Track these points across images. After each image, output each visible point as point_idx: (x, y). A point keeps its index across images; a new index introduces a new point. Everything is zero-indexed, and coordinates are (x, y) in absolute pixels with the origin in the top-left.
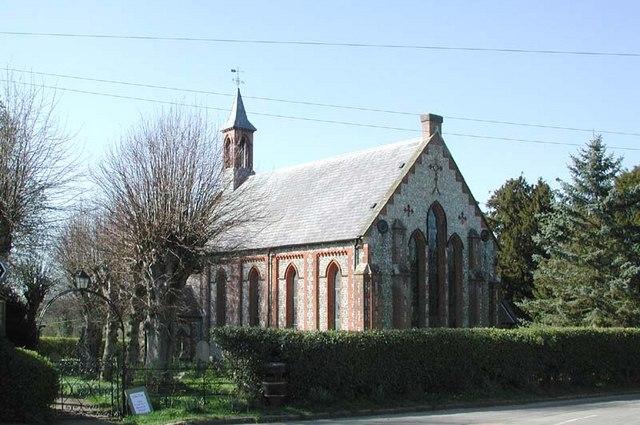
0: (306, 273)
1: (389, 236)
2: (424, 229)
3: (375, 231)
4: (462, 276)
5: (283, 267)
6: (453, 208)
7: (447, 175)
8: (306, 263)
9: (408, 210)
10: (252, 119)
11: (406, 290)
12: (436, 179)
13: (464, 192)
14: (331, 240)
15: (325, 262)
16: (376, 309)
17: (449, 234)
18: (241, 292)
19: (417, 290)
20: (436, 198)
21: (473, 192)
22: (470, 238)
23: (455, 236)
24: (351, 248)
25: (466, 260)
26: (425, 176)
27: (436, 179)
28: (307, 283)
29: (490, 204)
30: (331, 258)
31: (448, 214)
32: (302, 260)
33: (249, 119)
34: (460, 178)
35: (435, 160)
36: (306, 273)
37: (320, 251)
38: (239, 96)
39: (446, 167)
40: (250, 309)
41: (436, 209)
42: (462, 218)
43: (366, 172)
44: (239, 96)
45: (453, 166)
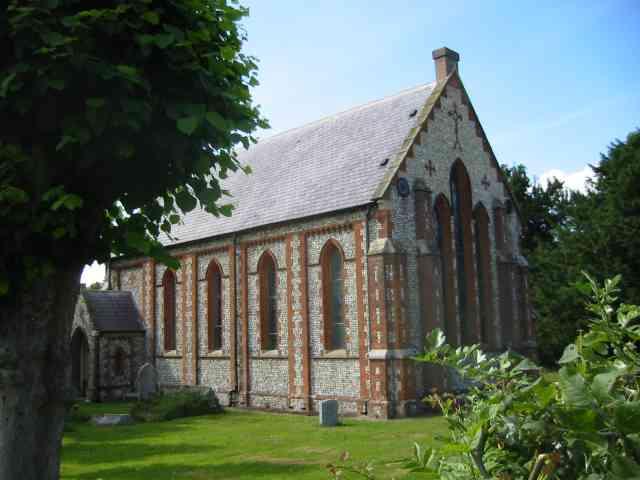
0: (289, 262)
1: (411, 199)
2: (448, 195)
3: (394, 195)
8: (289, 250)
9: (430, 168)
12: (456, 131)
18: (197, 295)
22: (496, 210)
27: (456, 131)
28: (290, 276)
34: (481, 133)
37: (306, 227)
39: (466, 117)
41: (458, 173)
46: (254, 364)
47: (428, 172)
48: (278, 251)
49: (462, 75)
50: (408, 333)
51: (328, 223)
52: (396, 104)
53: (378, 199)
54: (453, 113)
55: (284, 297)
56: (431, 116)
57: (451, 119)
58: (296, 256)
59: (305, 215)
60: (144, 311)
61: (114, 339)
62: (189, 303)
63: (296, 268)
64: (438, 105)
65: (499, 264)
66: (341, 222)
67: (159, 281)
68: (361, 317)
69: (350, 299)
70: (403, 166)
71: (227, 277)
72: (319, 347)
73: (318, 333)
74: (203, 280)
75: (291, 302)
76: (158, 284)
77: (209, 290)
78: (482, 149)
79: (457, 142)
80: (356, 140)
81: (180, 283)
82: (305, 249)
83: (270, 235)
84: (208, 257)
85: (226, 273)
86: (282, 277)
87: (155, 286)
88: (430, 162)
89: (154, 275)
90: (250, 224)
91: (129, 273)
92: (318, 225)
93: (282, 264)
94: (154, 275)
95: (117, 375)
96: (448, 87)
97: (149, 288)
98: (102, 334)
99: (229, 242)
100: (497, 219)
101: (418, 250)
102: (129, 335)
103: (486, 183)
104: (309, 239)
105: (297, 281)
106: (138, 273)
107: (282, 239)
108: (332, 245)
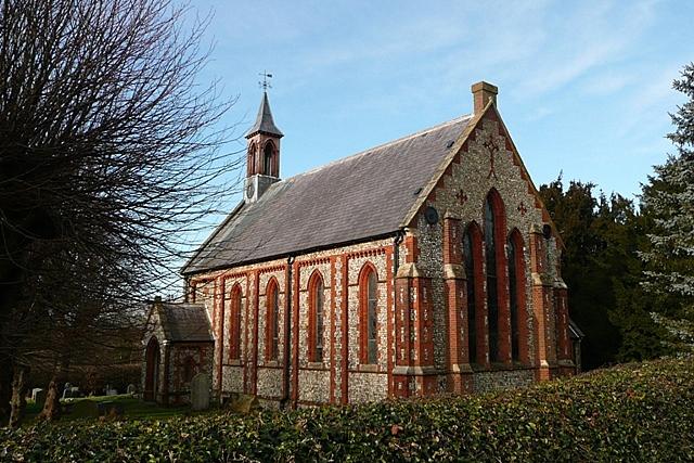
0: (334, 281)
2: (480, 222)
3: (421, 223)
5: (306, 274)
6: (507, 186)
7: (503, 155)
10: (279, 123)
12: (492, 161)
14: (365, 236)
15: (356, 265)
16: (423, 324)
24: (390, 241)
26: (478, 157)
27: (492, 161)
28: (334, 294)
30: (363, 259)
32: (328, 265)
33: (275, 124)
34: (518, 161)
35: (489, 132)
36: (334, 281)
37: (348, 249)
38: (266, 97)
39: (502, 148)
41: (493, 199)
43: (406, 159)
44: (266, 97)
45: (510, 146)
46: (302, 375)
47: (459, 201)
48: (243, 282)
49: (499, 108)
50: (74, 116)
52: (438, 135)
54: (491, 145)
55: (328, 314)
56: (465, 147)
58: (339, 276)
61: (185, 348)
62: (251, 316)
63: (339, 288)
64: (472, 136)
67: (262, 290)
68: (389, 334)
70: (431, 196)
72: (355, 360)
73: (354, 348)
80: (401, 168)
85: (282, 290)
86: (327, 294)
88: (462, 191)
92: (357, 248)
93: (327, 283)
95: (186, 381)
96: (203, 402)
97: (219, 301)
98: (171, 344)
103: (522, 209)
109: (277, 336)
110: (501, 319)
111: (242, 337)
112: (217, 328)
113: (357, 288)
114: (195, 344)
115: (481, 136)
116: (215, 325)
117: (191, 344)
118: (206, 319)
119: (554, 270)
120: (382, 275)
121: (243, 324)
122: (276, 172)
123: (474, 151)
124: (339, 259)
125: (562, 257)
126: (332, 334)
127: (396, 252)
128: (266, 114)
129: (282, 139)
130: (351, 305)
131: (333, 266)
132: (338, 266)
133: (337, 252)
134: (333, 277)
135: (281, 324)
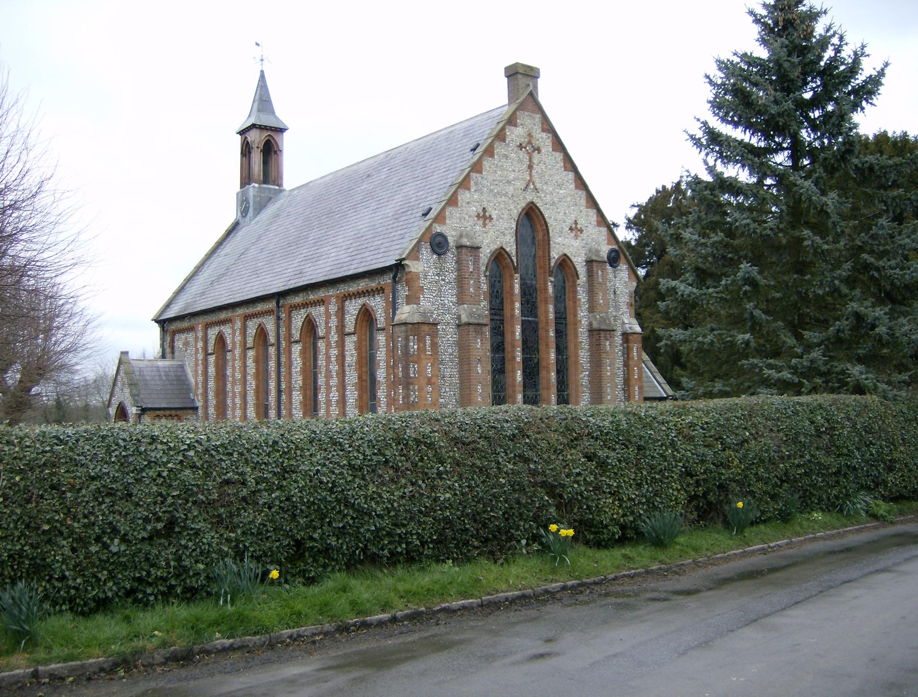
0: (328, 329)
1: (450, 258)
2: (511, 249)
4: (576, 323)
8: (328, 315)
9: (484, 217)
10: (283, 112)
11: (481, 346)
12: (530, 167)
13: (577, 187)
17: (555, 255)
18: (245, 366)
19: (499, 348)
20: (530, 197)
21: (557, 130)
22: (590, 262)
23: (565, 262)
24: (387, 280)
25: (582, 296)
27: (530, 167)
28: (328, 346)
29: (631, 224)
30: (361, 301)
31: (550, 222)
32: (322, 309)
34: (570, 164)
36: (328, 329)
37: (344, 289)
40: (257, 392)
42: (576, 229)
47: (481, 222)
48: (318, 312)
51: (362, 285)
53: (404, 259)
54: (529, 147)
55: (323, 370)
57: (522, 154)
59: (300, 284)
60: (197, 384)
62: (238, 376)
65: (592, 331)
66: (373, 285)
69: (381, 374)
71: (272, 345)
74: (296, 342)
75: (328, 376)
76: (248, 346)
77: (256, 361)
78: (572, 186)
79: (531, 181)
81: (229, 351)
82: (341, 312)
83: (311, 297)
84: (303, 311)
87: (207, 354)
89: (206, 340)
90: (292, 284)
91: (183, 336)
92: (353, 288)
94: (206, 340)
97: (201, 356)
99: (271, 305)
100: (590, 274)
101: (459, 317)
102: (178, 412)
103: (576, 229)
104: (347, 303)
105: (334, 352)
106: (190, 336)
107: (321, 302)
108: (367, 310)
109: (268, 401)
110: (543, 373)
111: (229, 402)
112: (200, 391)
113: (354, 338)
114: (173, 412)
115: (516, 134)
116: (197, 389)
117: (168, 413)
118: (187, 380)
119: (624, 308)
120: (381, 321)
121: (229, 386)
122: (278, 181)
123: (506, 157)
124: (333, 300)
125: (635, 291)
126: (328, 395)
127: (394, 292)
128: (263, 100)
129: (285, 134)
130: (348, 359)
131: (327, 310)
132: (333, 308)
133: (332, 292)
134: (327, 323)
135: (272, 385)
